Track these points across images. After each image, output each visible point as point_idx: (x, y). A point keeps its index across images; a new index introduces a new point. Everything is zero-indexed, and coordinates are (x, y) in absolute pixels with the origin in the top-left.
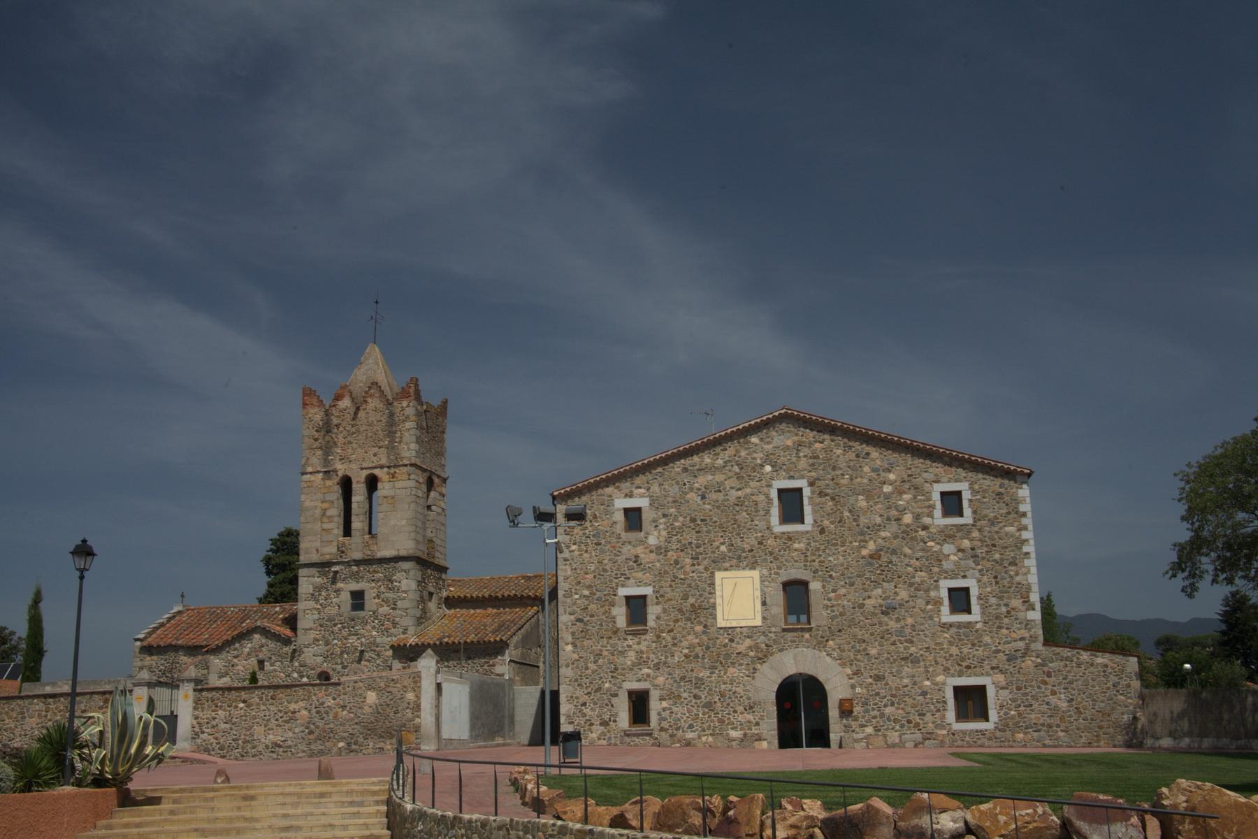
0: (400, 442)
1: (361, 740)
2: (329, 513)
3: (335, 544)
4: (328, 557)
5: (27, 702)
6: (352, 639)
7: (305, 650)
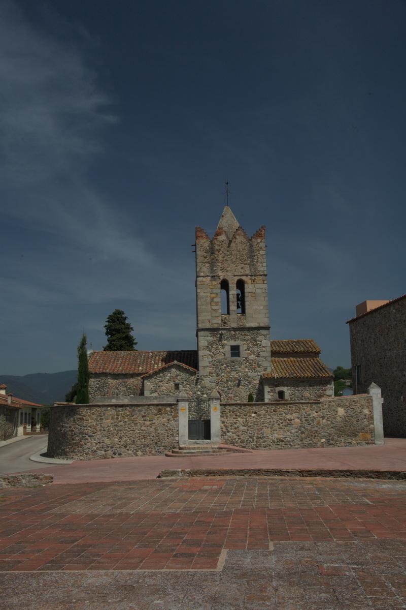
0: (257, 262)
1: (336, 437)
2: (215, 300)
3: (220, 318)
4: (216, 325)
5: (103, 409)
6: (233, 373)
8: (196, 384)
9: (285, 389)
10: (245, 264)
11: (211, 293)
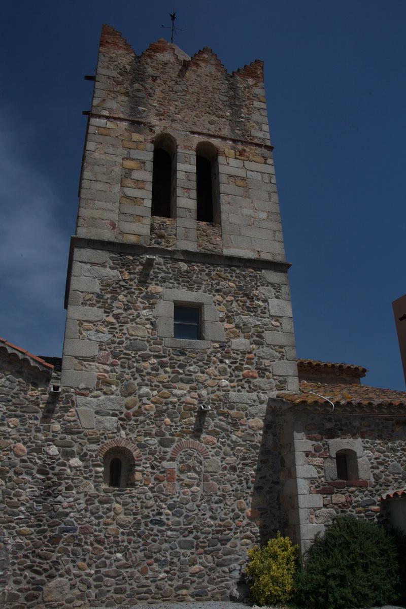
2: (136, 175)
6: (181, 390)
7: (80, 399)
8: (46, 418)
9: (356, 444)
10: (218, 116)
11: (125, 159)
